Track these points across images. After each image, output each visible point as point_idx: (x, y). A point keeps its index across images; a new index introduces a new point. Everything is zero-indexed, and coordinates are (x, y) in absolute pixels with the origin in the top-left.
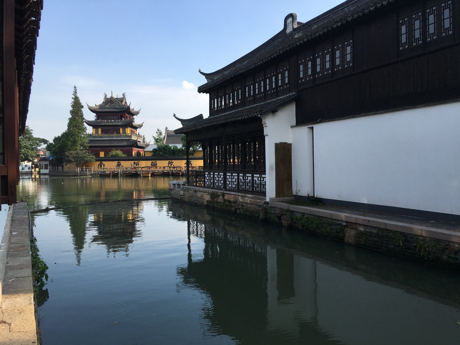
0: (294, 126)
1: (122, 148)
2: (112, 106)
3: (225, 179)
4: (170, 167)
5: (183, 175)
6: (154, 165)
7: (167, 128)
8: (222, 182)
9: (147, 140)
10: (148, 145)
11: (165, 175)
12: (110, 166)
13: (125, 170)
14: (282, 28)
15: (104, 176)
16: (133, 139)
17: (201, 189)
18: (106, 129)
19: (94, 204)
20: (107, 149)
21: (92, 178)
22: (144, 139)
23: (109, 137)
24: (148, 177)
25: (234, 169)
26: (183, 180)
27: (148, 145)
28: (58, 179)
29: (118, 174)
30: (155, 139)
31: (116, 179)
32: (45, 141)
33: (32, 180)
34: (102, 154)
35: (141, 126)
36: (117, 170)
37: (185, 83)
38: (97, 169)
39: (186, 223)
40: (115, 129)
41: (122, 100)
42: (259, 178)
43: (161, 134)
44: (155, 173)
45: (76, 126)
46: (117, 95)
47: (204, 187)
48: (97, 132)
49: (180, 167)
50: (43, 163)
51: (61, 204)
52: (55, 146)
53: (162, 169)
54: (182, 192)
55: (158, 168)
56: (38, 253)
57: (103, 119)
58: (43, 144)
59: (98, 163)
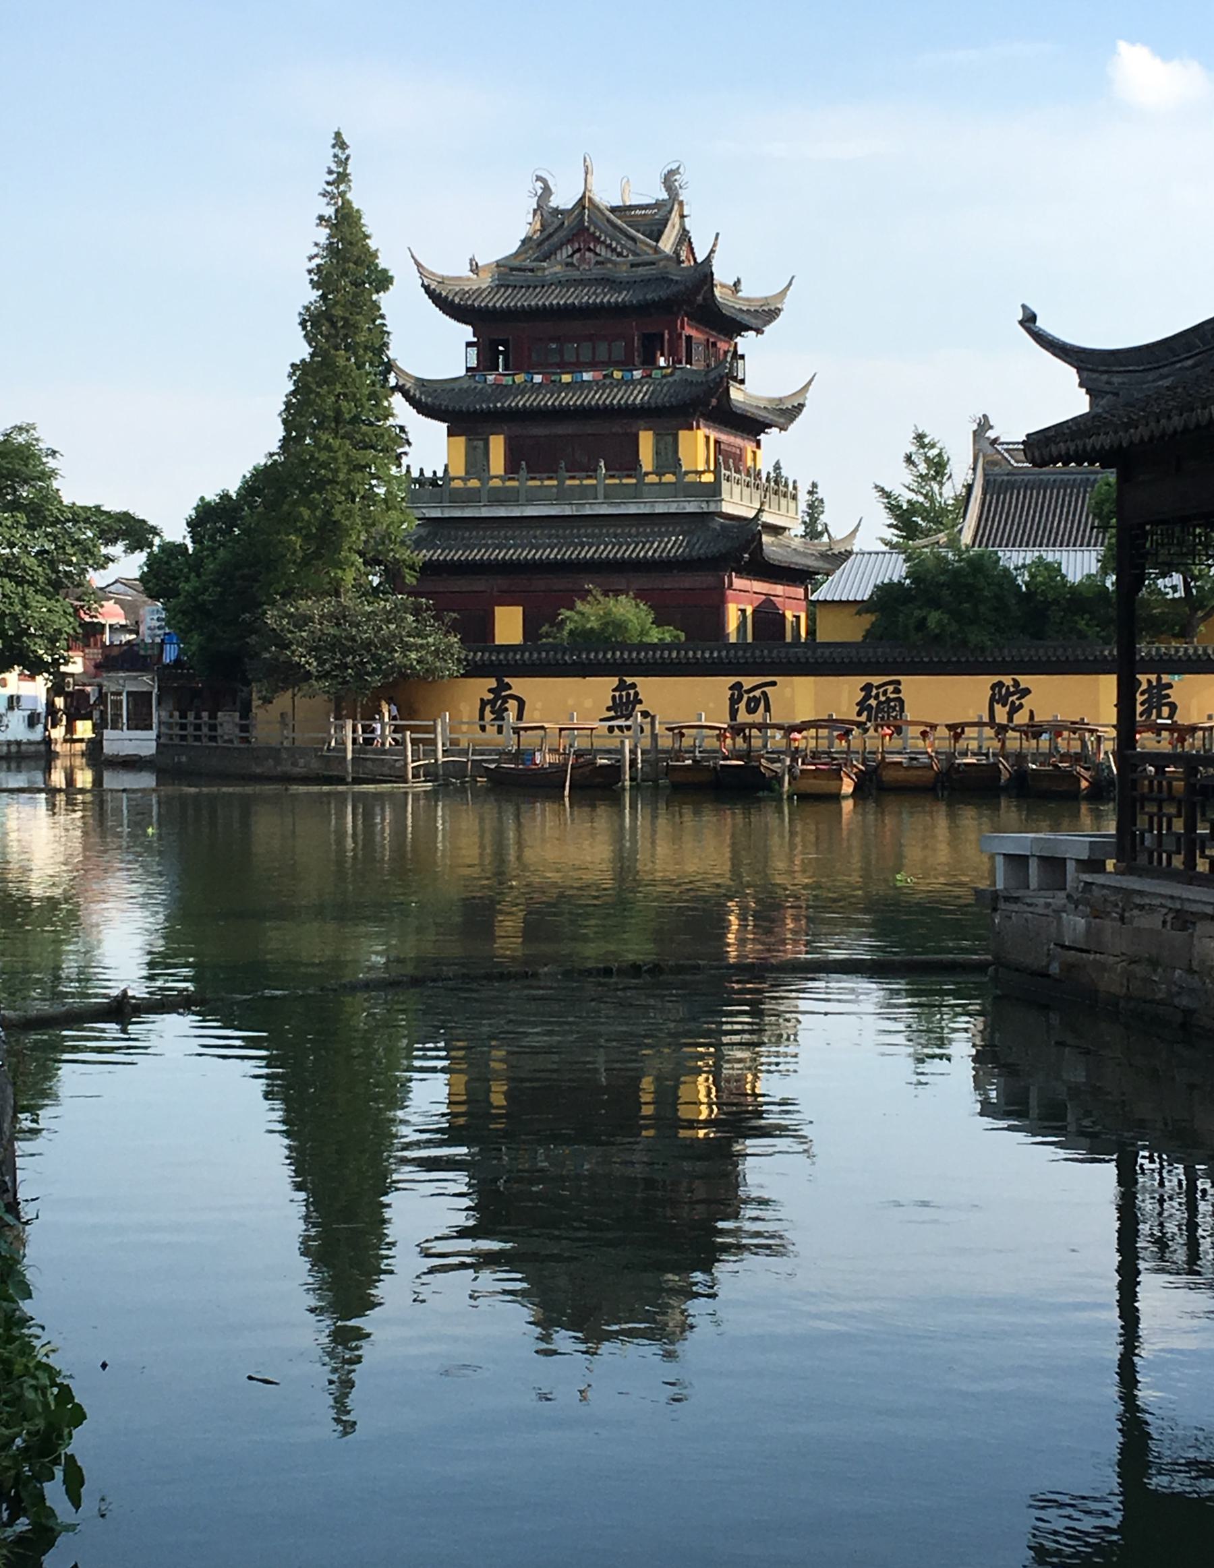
1: (643, 581)
2: (588, 267)
4: (1001, 729)
5: (1098, 792)
6: (884, 711)
7: (984, 425)
9: (836, 522)
10: (838, 558)
11: (961, 786)
12: (565, 711)
13: (666, 742)
15: (517, 783)
16: (727, 508)
18: (548, 441)
19: (456, 988)
20: (546, 586)
21: (435, 791)
22: (815, 508)
23: (562, 496)
24: (836, 797)
26: (1096, 828)
27: (838, 558)
28: (212, 800)
29: (614, 771)
30: (894, 508)
31: (602, 811)
32: (133, 531)
33: (52, 806)
34: (509, 625)
35: (787, 413)
36: (613, 743)
37: (1140, 71)
38: (469, 735)
39: (1108, 1171)
40: (600, 437)
41: (653, 219)
43: (939, 467)
44: (888, 775)
45: (338, 417)
46: (624, 184)
48: (476, 462)
49: (1077, 727)
50: (124, 684)
51: (228, 972)
52: (196, 563)
53: (941, 741)
54: (1076, 924)
55: (914, 731)
56: (27, 1307)
57: (519, 369)
58: (117, 550)
59: (483, 686)
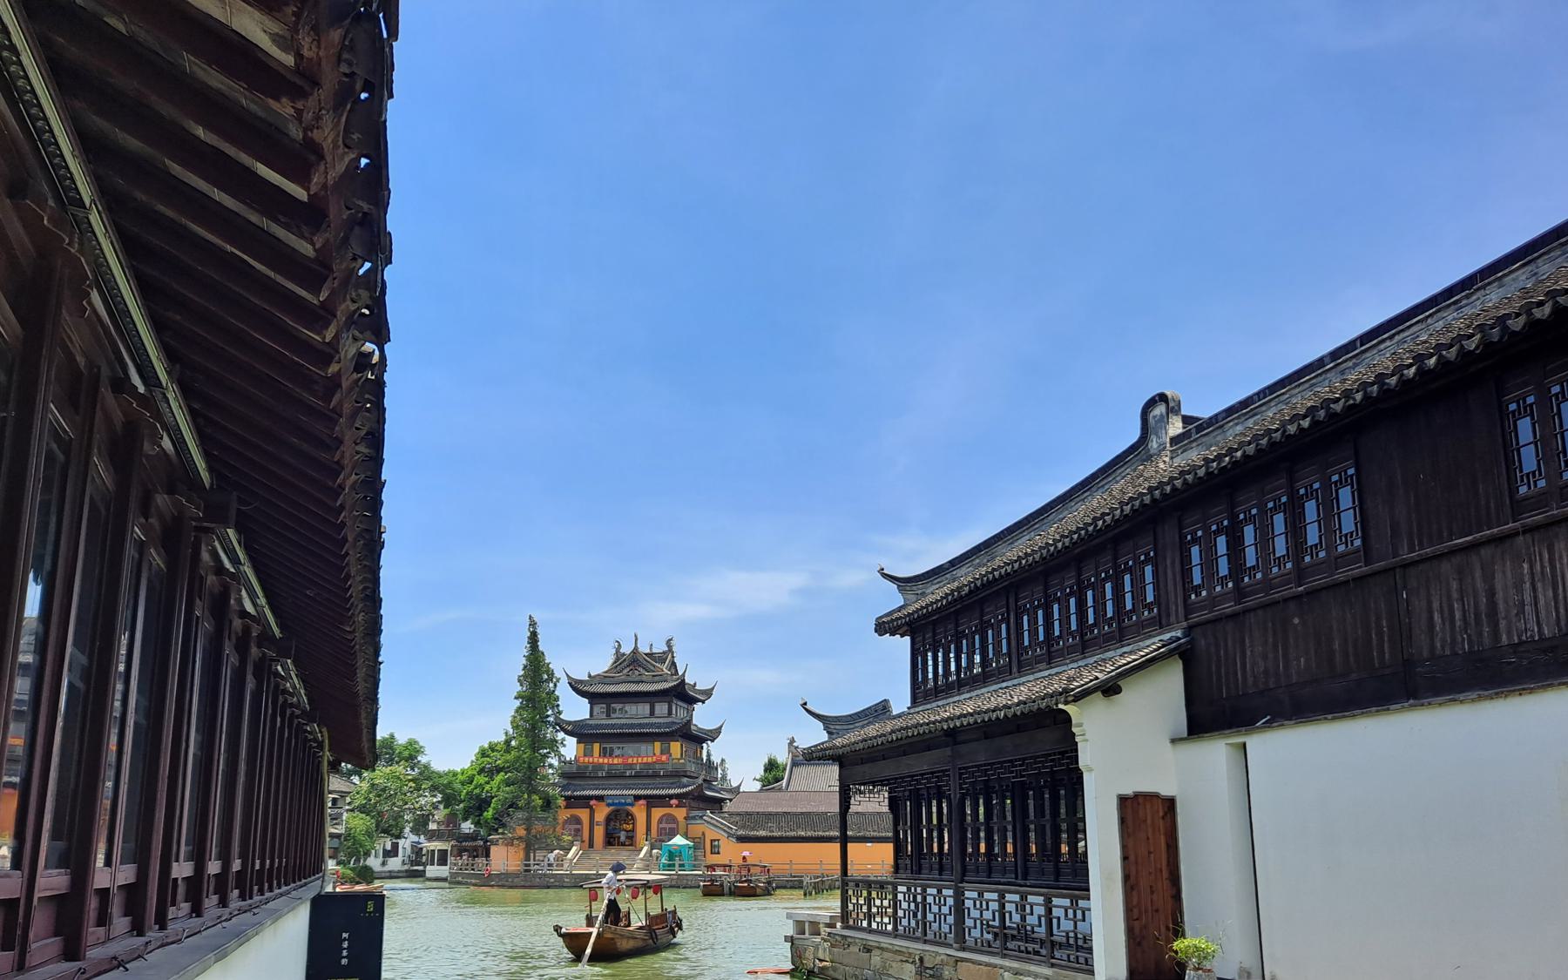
0: (1182, 739)
1: (889, 769)
3: (959, 910)
7: (792, 741)
8: (951, 919)
14: (1134, 435)
17: (885, 941)
25: (989, 871)
42: (1070, 912)
47: (895, 934)
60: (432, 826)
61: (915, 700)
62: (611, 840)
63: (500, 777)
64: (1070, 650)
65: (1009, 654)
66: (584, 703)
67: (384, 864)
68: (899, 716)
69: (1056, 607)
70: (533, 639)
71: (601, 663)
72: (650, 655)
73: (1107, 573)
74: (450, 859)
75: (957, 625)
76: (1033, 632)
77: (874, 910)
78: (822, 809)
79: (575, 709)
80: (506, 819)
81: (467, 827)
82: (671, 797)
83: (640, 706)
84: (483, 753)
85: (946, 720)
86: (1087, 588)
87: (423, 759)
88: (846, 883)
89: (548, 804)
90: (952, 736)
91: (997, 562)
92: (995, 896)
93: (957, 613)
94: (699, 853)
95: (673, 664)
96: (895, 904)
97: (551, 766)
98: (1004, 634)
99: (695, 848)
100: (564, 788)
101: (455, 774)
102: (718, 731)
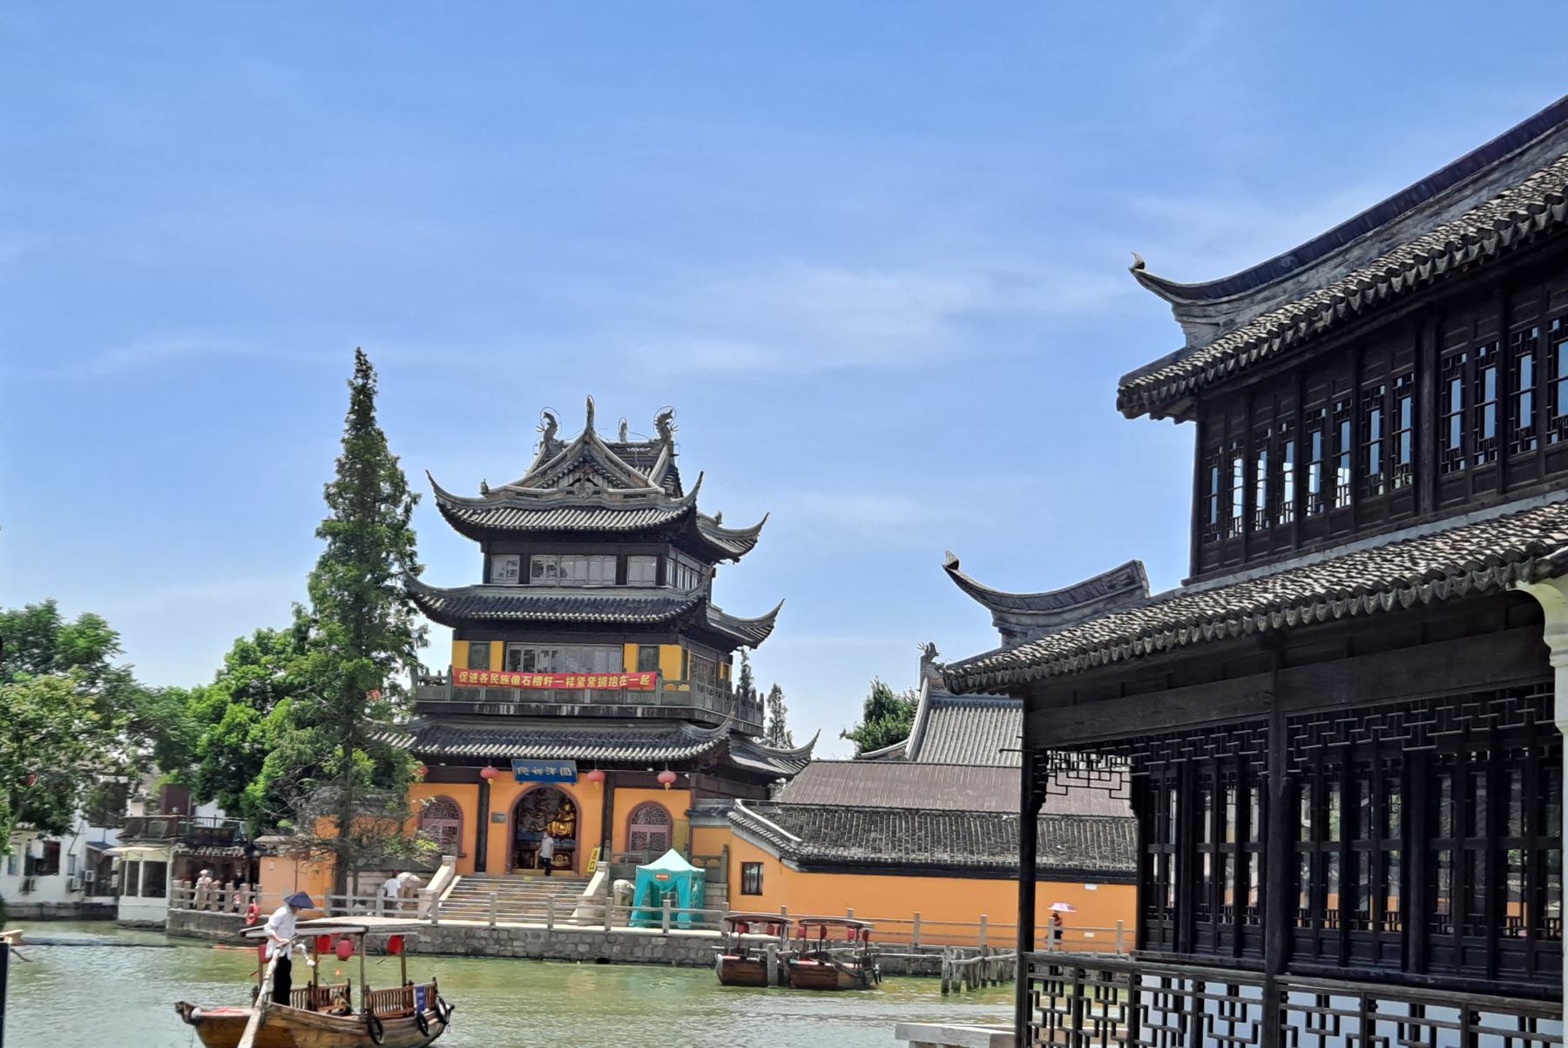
1: (1131, 718)
7: (931, 652)
42: (1316, 1018)
46: (624, 420)
48: (477, 662)
60: (134, 810)
61: (1200, 567)
62: (522, 855)
63: (279, 710)
64: (1479, 482)
65: (1415, 467)
66: (474, 551)
67: (27, 888)
68: (1164, 599)
69: (1527, 363)
70: (363, 402)
71: (514, 465)
72: (620, 449)
73: (1490, 347)
74: (172, 884)
75: (1303, 400)
76: (1473, 418)
77: (1088, 1026)
78: (991, 805)
79: (452, 563)
80: (294, 800)
81: (210, 814)
82: (659, 765)
83: (596, 562)
84: (244, 656)
85: (1266, 610)
86: (1522, 349)
87: (114, 661)
88: (1029, 969)
89: (387, 771)
90: (1278, 646)
91: (1402, 255)
92: (1354, 1004)
93: (1304, 372)
94: (716, 891)
95: (672, 472)
96: (1135, 1014)
97: (395, 688)
98: (1406, 422)
99: (708, 880)
100: (423, 737)
101: (183, 699)
102: (767, 624)
